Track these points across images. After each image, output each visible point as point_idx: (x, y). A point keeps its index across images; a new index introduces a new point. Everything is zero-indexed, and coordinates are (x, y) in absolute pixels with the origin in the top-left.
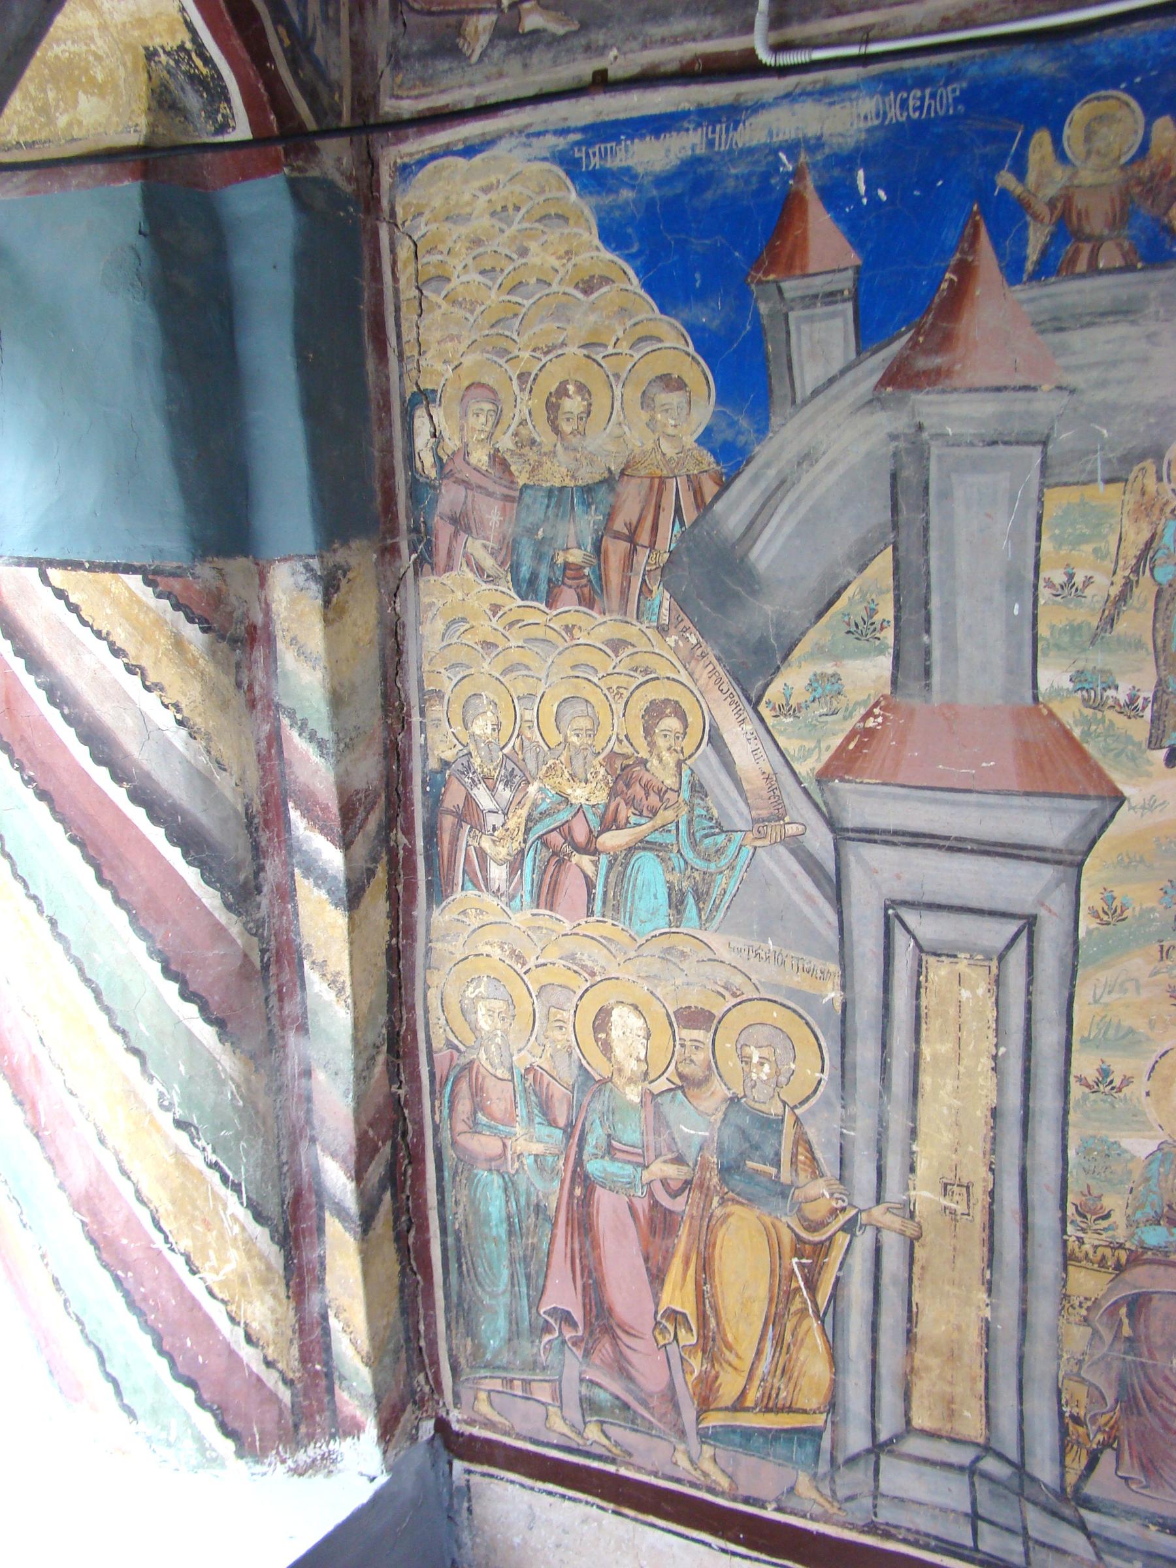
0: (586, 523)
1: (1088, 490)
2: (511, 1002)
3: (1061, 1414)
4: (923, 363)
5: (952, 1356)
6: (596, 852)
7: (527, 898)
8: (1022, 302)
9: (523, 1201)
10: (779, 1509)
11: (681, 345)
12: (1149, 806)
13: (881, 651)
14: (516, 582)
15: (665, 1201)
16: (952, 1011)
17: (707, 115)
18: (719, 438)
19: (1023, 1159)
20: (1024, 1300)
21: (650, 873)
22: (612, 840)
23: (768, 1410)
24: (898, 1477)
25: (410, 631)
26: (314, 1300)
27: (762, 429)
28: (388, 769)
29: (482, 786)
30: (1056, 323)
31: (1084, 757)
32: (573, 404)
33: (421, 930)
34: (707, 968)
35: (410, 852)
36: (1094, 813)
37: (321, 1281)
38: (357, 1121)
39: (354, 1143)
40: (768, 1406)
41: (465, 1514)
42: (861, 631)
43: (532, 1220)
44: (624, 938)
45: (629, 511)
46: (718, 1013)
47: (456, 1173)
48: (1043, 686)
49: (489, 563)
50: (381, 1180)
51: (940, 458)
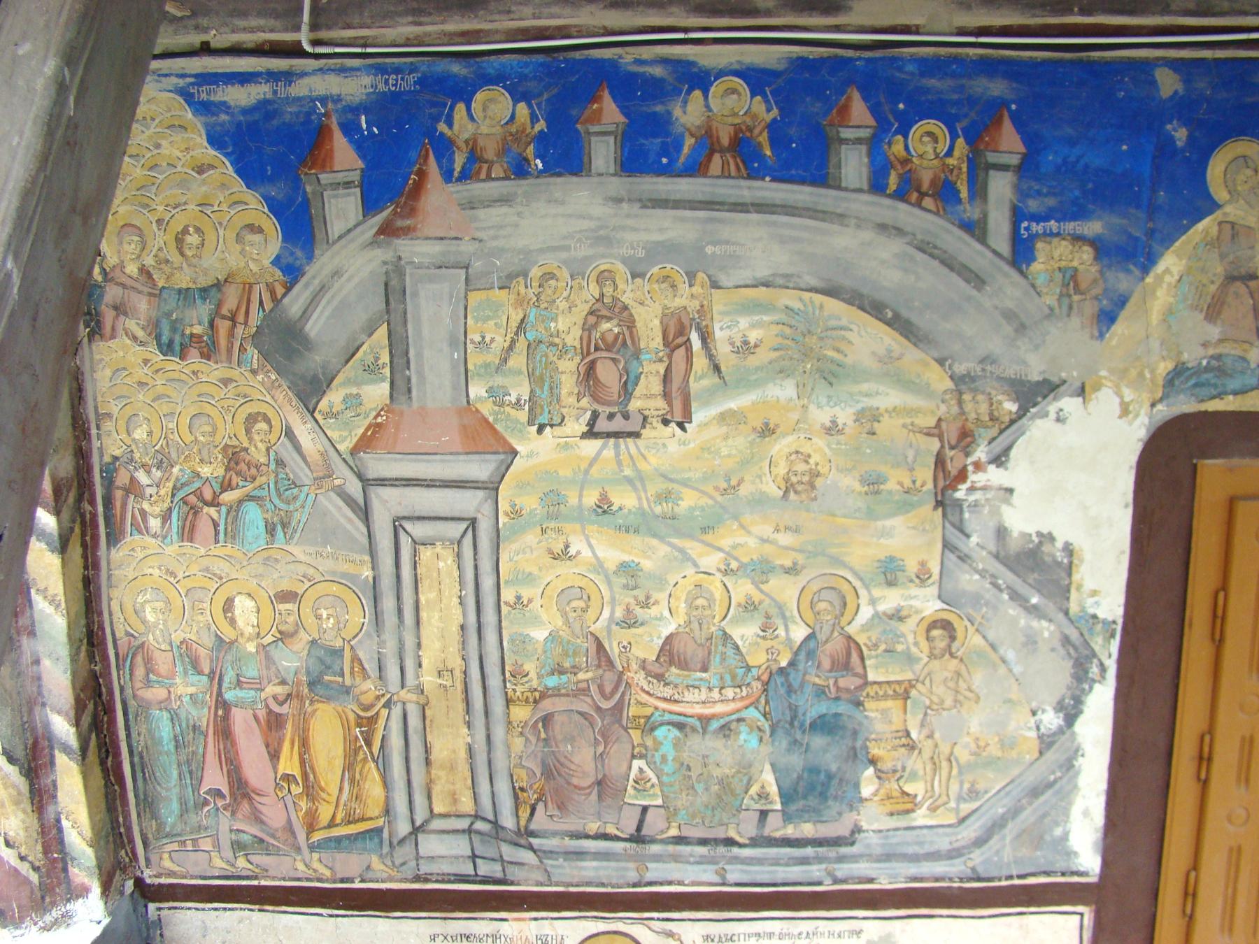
0: (204, 310)
1: (491, 292)
2: (168, 602)
3: (514, 788)
4: (400, 223)
5: (452, 768)
6: (218, 505)
7: (175, 537)
8: (452, 193)
9: (184, 725)
10: (363, 881)
11: (260, 207)
12: (530, 455)
13: (383, 380)
14: (159, 345)
15: (276, 708)
16: (435, 575)
17: (272, 76)
18: (284, 261)
19: (480, 651)
20: (488, 729)
21: (253, 514)
22: (228, 497)
23: (349, 822)
24: (430, 845)
25: (87, 376)
26: (50, 811)
27: (310, 257)
28: (78, 463)
29: (141, 471)
30: (471, 205)
31: (495, 430)
32: (193, 239)
33: (103, 564)
34: (292, 566)
35: (94, 516)
36: (502, 461)
37: (55, 797)
38: (74, 688)
39: (72, 701)
40: (349, 821)
41: (158, 938)
42: (371, 370)
43: (192, 735)
44: (239, 555)
45: (231, 303)
46: (300, 592)
47: (137, 715)
48: (472, 395)
49: (140, 334)
50: (90, 725)
51: (411, 274)
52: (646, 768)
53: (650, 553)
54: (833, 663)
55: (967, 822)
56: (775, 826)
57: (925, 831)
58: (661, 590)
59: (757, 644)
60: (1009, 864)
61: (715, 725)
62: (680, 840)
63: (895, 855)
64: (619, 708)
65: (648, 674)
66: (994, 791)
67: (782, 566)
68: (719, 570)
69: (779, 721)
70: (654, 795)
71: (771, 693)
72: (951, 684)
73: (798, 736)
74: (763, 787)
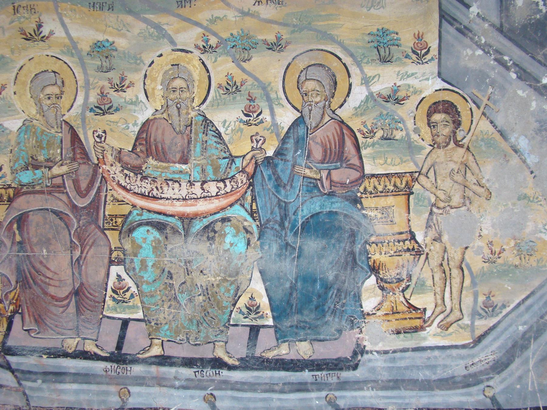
52: (124, 275)
53: (124, 31)
54: (325, 151)
55: (485, 342)
56: (268, 346)
57: (436, 353)
58: (137, 71)
59: (241, 130)
60: (534, 393)
61: (198, 226)
62: (163, 360)
63: (403, 381)
64: (95, 206)
65: (125, 166)
66: (512, 306)
67: (265, 42)
68: (197, 47)
69: (268, 221)
70: (134, 307)
71: (258, 188)
72: (459, 178)
73: (290, 239)
74: (252, 298)
